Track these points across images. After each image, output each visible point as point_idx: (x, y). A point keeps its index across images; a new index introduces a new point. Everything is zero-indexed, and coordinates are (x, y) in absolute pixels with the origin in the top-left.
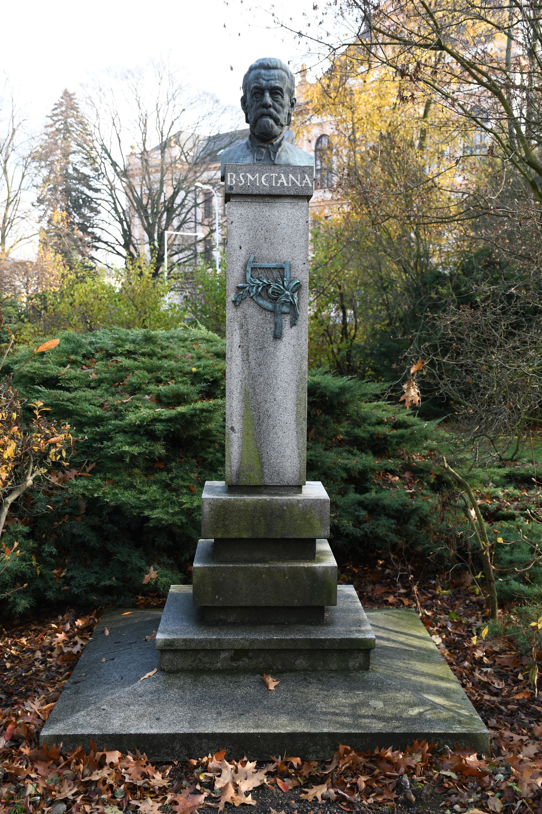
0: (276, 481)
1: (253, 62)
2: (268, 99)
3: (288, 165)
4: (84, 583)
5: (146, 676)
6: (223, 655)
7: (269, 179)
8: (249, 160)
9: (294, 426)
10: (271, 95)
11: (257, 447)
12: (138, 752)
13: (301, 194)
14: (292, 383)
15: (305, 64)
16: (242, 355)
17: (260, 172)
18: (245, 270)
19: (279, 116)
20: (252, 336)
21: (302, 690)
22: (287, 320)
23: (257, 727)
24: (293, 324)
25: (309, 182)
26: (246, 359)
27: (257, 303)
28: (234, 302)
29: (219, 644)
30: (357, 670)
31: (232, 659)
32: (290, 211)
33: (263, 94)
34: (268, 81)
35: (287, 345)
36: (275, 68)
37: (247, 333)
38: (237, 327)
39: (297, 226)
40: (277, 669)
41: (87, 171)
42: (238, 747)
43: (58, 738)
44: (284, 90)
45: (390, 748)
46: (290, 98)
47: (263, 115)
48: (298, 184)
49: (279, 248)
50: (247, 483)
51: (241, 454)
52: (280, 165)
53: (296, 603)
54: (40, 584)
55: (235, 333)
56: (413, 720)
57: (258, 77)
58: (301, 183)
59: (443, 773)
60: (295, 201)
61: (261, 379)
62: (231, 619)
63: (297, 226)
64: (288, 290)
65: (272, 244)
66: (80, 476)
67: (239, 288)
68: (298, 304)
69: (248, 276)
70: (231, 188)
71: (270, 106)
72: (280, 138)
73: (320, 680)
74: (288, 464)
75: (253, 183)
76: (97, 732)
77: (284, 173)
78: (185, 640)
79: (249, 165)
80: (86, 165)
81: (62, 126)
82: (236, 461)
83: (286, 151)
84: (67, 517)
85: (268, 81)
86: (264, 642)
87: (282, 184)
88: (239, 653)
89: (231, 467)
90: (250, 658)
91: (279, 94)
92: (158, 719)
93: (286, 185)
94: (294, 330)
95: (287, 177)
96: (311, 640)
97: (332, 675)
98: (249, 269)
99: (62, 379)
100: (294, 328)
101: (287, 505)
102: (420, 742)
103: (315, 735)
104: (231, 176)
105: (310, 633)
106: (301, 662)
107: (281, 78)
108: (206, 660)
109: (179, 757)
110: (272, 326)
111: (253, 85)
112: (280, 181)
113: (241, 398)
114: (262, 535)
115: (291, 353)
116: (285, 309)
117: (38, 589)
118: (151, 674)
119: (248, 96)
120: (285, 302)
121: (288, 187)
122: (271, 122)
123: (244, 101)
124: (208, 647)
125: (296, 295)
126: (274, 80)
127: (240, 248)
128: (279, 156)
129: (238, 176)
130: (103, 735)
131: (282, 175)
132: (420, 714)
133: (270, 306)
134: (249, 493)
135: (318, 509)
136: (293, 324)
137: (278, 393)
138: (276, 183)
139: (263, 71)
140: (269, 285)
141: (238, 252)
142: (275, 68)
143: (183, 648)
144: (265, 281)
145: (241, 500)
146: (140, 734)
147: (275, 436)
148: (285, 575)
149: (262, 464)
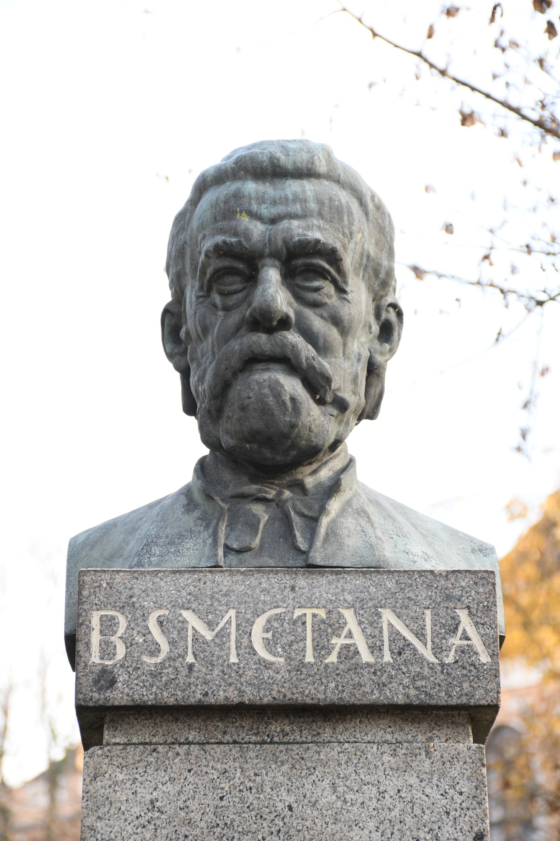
1: (214, 155)
2: (275, 292)
3: (374, 569)
7: (284, 634)
8: (193, 551)
10: (289, 276)
13: (442, 699)
19: (325, 364)
25: (477, 642)
32: (391, 785)
33: (252, 277)
34: (274, 221)
36: (305, 173)
44: (349, 261)
46: (377, 298)
47: (254, 360)
48: (427, 653)
52: (338, 570)
57: (227, 212)
58: (438, 650)
60: (415, 735)
70: (106, 679)
71: (284, 323)
72: (336, 464)
79: (193, 570)
83: (362, 513)
87: (349, 653)
91: (323, 274)
93: (366, 657)
104: (108, 625)
107: (334, 213)
111: (208, 245)
112: (338, 642)
119: (190, 295)
121: (376, 670)
122: (292, 386)
123: (173, 322)
126: (303, 216)
128: (332, 532)
129: (138, 617)
131: (349, 615)
138: (322, 648)
139: (251, 187)
142: (305, 173)
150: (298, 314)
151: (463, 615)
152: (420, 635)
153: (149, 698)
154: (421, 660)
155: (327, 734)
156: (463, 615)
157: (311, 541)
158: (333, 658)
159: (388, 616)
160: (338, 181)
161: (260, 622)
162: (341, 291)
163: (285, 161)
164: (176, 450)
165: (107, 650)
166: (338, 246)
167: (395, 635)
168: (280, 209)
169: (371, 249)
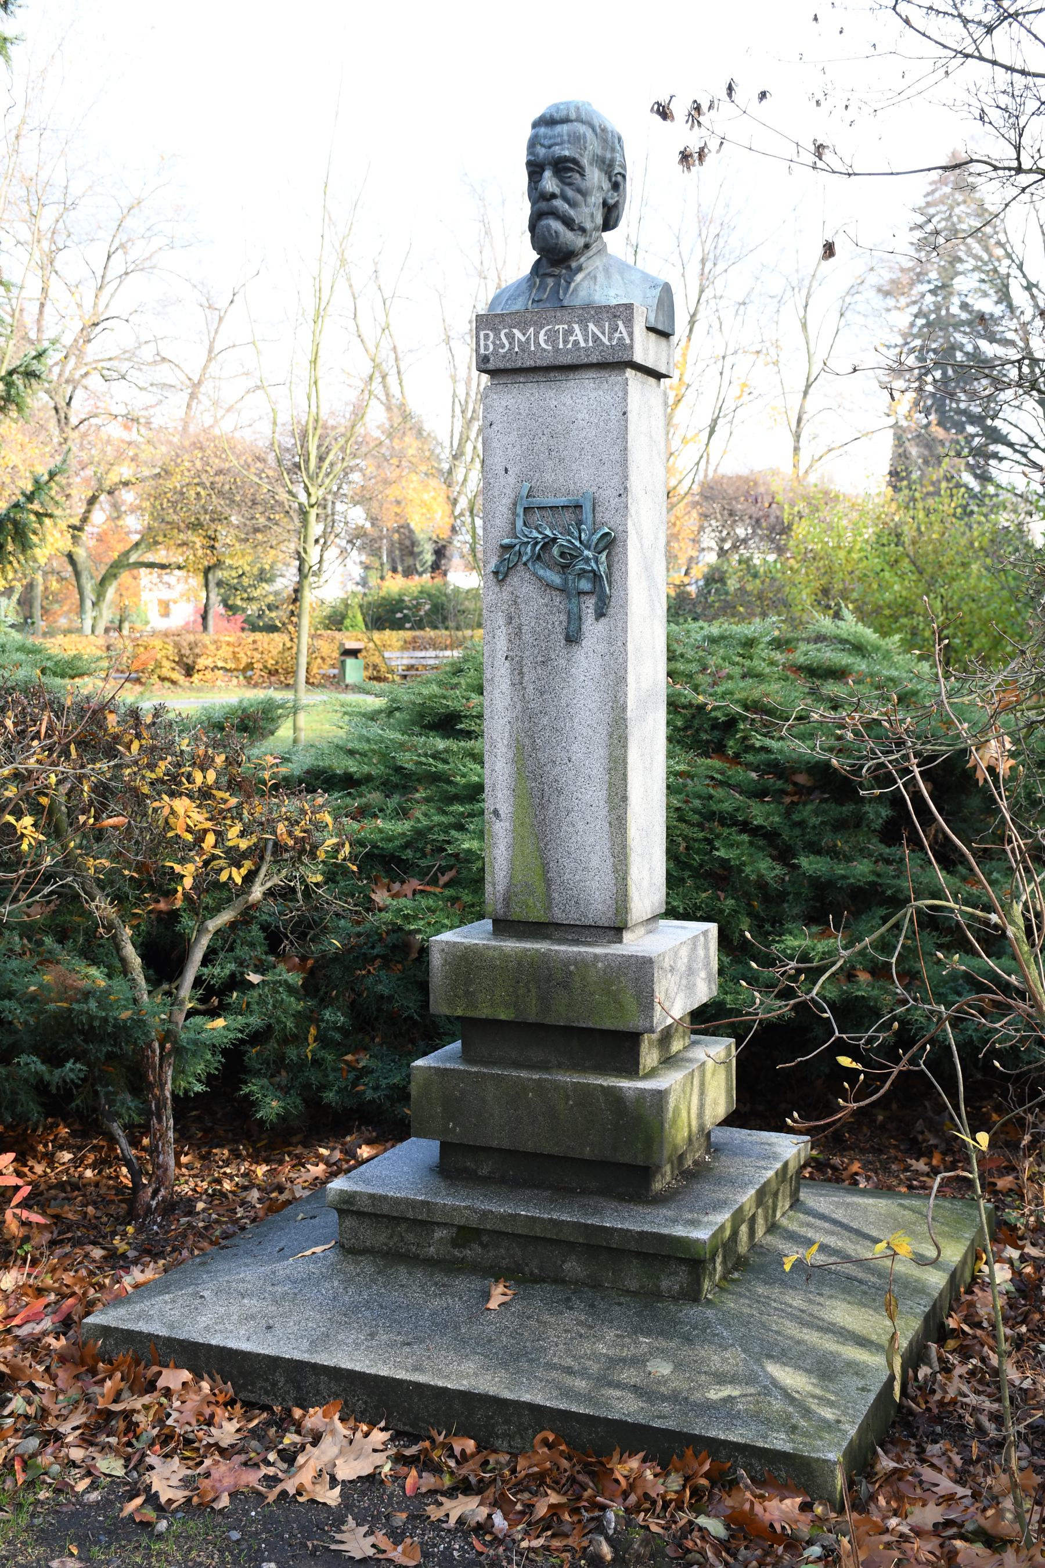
0: (572, 917)
1: (537, 112)
4: (384, 1083)
5: (308, 1253)
6: (439, 1234)
9: (605, 812)
11: (538, 849)
12: (218, 1377)
13: (611, 360)
14: (600, 729)
16: (512, 674)
17: (535, 324)
18: (514, 514)
19: (572, 213)
20: (527, 637)
21: (546, 1317)
22: (589, 604)
23: (416, 1369)
24: (600, 614)
26: (518, 683)
27: (535, 574)
29: (429, 1210)
30: (675, 1299)
31: (455, 1243)
32: (593, 395)
34: (550, 147)
35: (591, 654)
36: (566, 120)
37: (518, 633)
38: (501, 621)
39: (606, 422)
40: (532, 1273)
41: (987, 305)
42: (368, 1399)
43: (106, 1331)
44: (585, 162)
45: (641, 1454)
49: (574, 467)
50: (523, 917)
51: (512, 862)
52: (573, 308)
53: (587, 1152)
54: (313, 1077)
55: (498, 632)
56: (708, 1408)
58: (610, 339)
59: (702, 1521)
61: (545, 721)
62: (484, 1171)
63: (606, 422)
64: (588, 548)
65: (561, 460)
66: (422, 891)
68: (609, 575)
69: (519, 523)
71: (553, 196)
73: (592, 1306)
74: (595, 885)
75: (524, 347)
76: (163, 1332)
77: (580, 322)
78: (372, 1196)
80: (985, 295)
81: (943, 224)
82: (502, 874)
84: (378, 963)
85: (550, 147)
86: (503, 1218)
87: (576, 343)
88: (466, 1234)
89: (494, 885)
90: (484, 1246)
91: (571, 170)
92: (269, 1328)
93: (582, 344)
94: (602, 625)
95: (585, 330)
96: (586, 1225)
97: (622, 1300)
98: (520, 511)
99: (465, 717)
100: (603, 620)
101: (576, 963)
102: (696, 1455)
103: (505, 1402)
105: (597, 1212)
106: (572, 1267)
108: (410, 1237)
109: (284, 1400)
110: (563, 617)
112: (572, 339)
113: (510, 755)
114: (532, 1019)
115: (599, 670)
116: (585, 585)
117: (308, 1086)
118: (318, 1249)
120: (584, 571)
121: (586, 349)
124: (410, 1215)
125: (603, 557)
127: (506, 471)
128: (575, 290)
129: (497, 336)
130: (170, 1340)
131: (576, 327)
132: (730, 1399)
133: (557, 579)
134: (521, 936)
135: (631, 975)
136: (600, 614)
137: (575, 747)
138: (566, 342)
140: (554, 540)
142: (566, 120)
143: (369, 1210)
144: (548, 532)
145: (495, 948)
146: (224, 1348)
147: (571, 829)
148: (567, 1097)
149: (548, 882)
150: (562, 191)
151: (620, 323)
152: (603, 333)
153: (502, 367)
154: (603, 344)
155: (571, 376)
156: (620, 323)
157: (565, 294)
158: (570, 346)
159: (591, 326)
160: (582, 122)
161: (543, 332)
162: (582, 175)
163: (557, 116)
164: (525, 257)
165: (486, 347)
166: (577, 156)
167: (594, 333)
168: (552, 141)
169: (599, 152)
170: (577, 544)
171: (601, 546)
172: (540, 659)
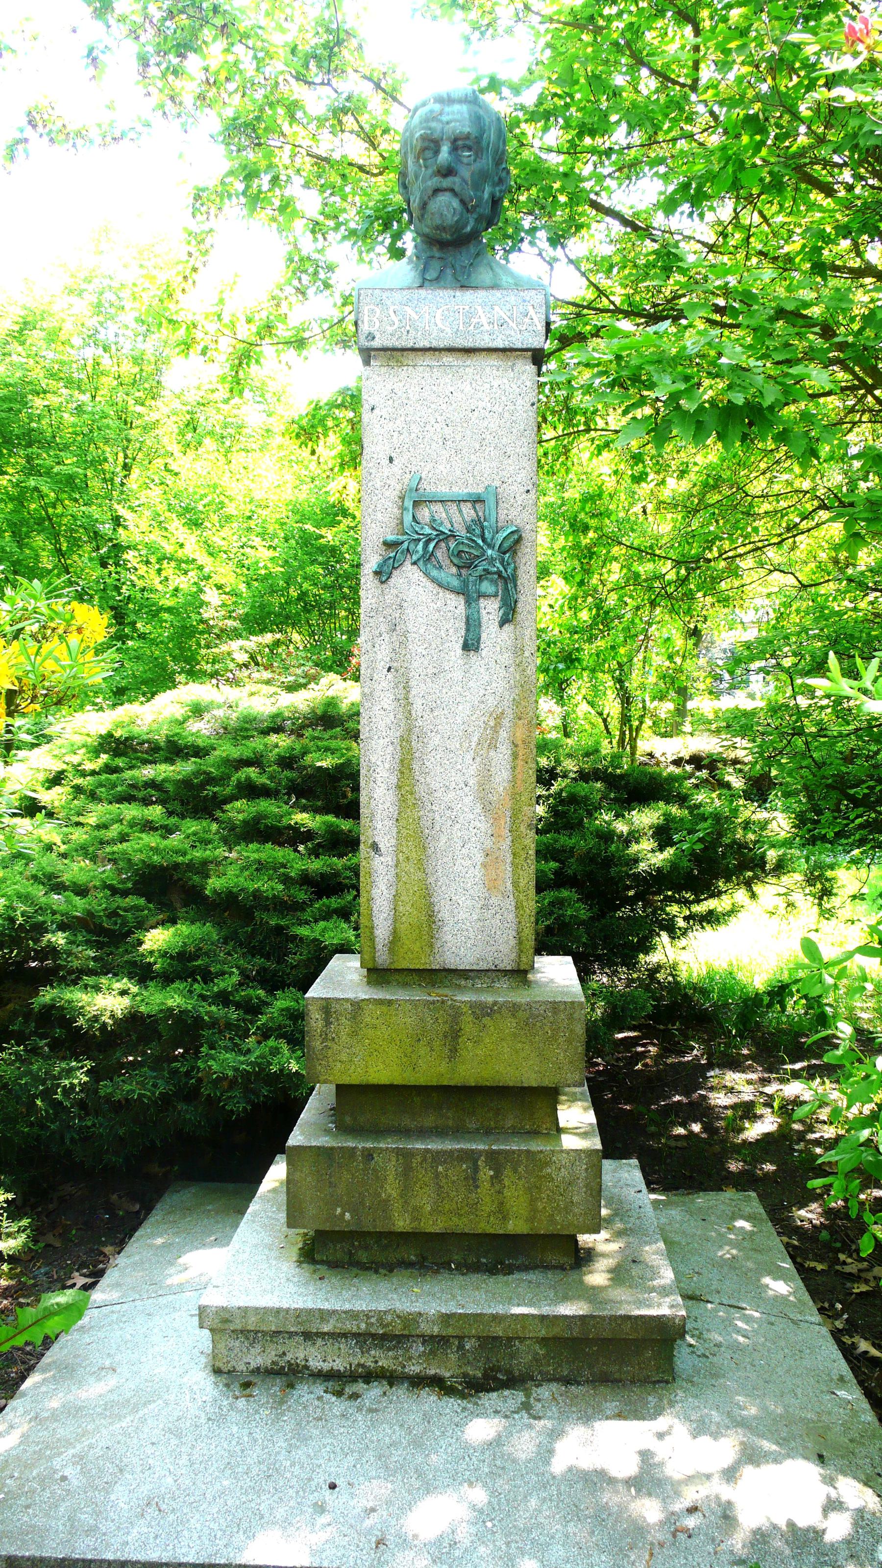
15: (421, 1537)
18: (403, 508)
28: (377, 573)
55: (378, 641)
64: (491, 546)
67: (389, 545)
98: (409, 504)
111: (417, 135)
127: (391, 460)
141: (387, 470)
170: (480, 542)
171: (506, 545)
172: (431, 670)
